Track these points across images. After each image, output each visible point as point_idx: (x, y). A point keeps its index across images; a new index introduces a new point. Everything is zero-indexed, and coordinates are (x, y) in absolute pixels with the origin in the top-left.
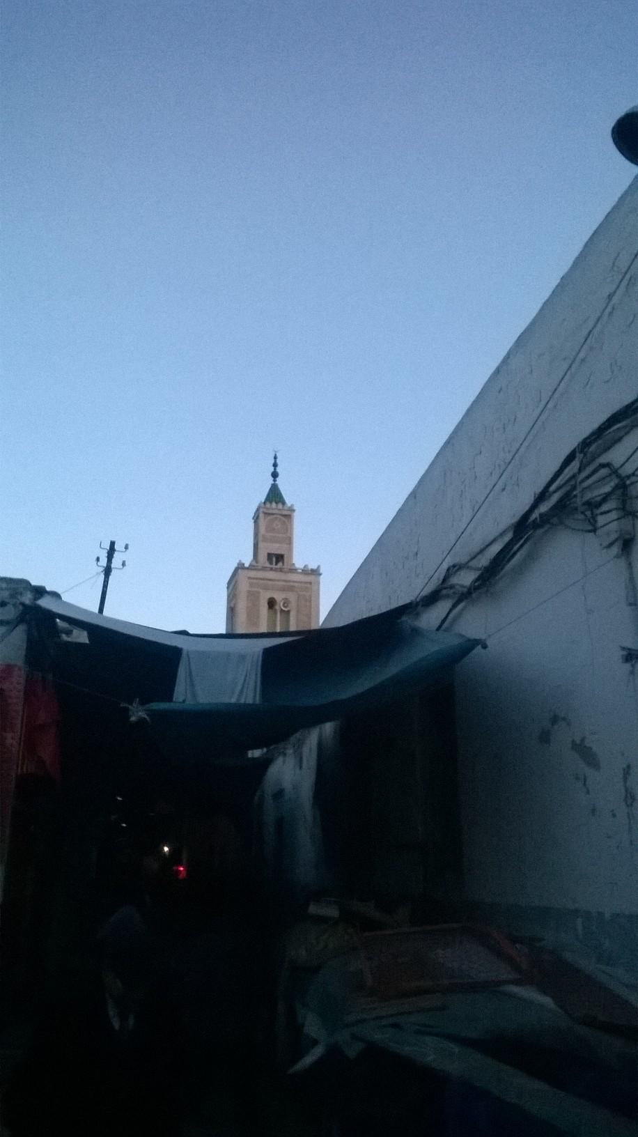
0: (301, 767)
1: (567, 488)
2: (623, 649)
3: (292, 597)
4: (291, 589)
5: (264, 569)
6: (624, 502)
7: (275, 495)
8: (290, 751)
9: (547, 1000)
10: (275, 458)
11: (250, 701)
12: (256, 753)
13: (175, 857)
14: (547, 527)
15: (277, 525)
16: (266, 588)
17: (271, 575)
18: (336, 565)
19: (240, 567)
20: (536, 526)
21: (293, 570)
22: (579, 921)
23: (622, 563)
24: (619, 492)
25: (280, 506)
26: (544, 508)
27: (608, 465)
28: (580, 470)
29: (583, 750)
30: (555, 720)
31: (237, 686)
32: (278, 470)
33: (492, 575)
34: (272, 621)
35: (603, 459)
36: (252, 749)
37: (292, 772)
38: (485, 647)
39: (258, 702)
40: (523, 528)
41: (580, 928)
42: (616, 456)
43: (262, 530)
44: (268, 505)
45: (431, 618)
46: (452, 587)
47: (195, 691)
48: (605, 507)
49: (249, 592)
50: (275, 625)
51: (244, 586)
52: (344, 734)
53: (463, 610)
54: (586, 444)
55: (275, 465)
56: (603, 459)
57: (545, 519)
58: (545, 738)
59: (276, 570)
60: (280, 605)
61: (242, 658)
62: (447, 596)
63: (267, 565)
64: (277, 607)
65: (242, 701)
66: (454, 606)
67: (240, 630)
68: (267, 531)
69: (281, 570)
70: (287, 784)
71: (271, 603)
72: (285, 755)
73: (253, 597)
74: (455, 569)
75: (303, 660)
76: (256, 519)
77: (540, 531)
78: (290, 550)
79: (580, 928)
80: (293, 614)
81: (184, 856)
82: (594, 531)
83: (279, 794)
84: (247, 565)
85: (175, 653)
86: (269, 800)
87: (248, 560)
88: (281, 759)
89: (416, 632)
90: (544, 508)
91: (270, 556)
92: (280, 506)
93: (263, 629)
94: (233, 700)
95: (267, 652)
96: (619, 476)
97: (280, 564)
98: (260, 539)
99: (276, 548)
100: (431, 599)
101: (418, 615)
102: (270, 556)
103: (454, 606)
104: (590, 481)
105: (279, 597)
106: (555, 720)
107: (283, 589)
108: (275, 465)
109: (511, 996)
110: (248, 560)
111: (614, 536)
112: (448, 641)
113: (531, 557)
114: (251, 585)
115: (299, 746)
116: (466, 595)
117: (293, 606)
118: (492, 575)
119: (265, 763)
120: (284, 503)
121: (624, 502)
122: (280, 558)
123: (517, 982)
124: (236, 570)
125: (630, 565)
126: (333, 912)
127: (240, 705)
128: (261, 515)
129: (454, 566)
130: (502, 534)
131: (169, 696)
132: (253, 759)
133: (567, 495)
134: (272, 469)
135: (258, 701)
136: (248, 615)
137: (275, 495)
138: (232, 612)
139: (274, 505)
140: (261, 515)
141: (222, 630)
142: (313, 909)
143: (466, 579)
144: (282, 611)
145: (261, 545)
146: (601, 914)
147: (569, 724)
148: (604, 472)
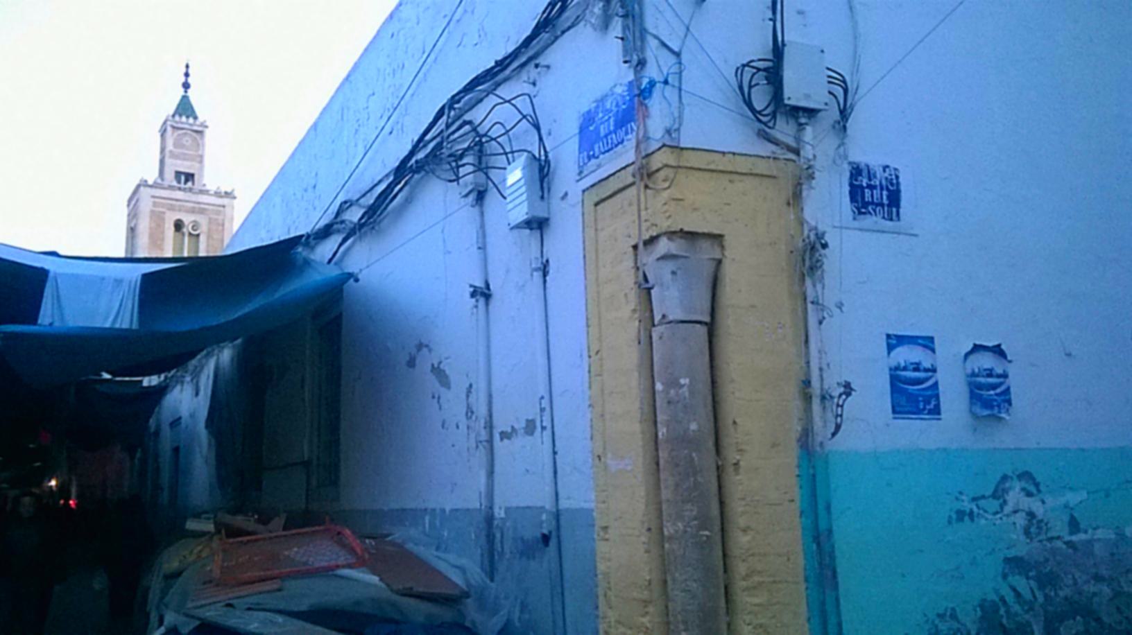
0: (197, 394)
1: (438, 139)
2: (471, 286)
3: (203, 221)
4: (202, 212)
5: (171, 188)
6: (480, 158)
7: (185, 108)
8: (188, 379)
9: (375, 579)
10: (187, 66)
11: (125, 326)
12: (150, 381)
13: (63, 490)
14: (423, 173)
15: (187, 141)
16: (172, 208)
17: (179, 195)
18: (247, 190)
19: (143, 184)
20: (420, 167)
21: (206, 192)
22: (427, 519)
23: (476, 210)
24: (477, 148)
25: (191, 120)
26: (420, 155)
27: (470, 123)
28: (448, 126)
29: (438, 371)
30: (420, 346)
31: (114, 311)
32: (190, 71)
33: (375, 213)
34: (179, 245)
35: (467, 117)
36: (150, 374)
37: (188, 400)
38: (357, 280)
39: (135, 326)
40: (402, 170)
41: (427, 521)
42: (477, 115)
43: (170, 146)
44: (177, 118)
45: (327, 248)
46: (342, 222)
47: (62, 313)
48: (465, 161)
49: (152, 212)
50: (182, 249)
51: (146, 206)
52: (244, 361)
53: (353, 243)
54: (454, 100)
55: (187, 75)
56: (467, 117)
57: (420, 167)
58: (411, 363)
59: (184, 190)
60: (187, 229)
61: (118, 282)
62: (339, 231)
63: (175, 183)
64: (185, 230)
65: (117, 326)
66: (345, 240)
67: (141, 254)
68: (175, 145)
69: (190, 190)
70: (184, 411)
71: (178, 226)
72: (182, 383)
73: (158, 218)
74: (346, 205)
75: (185, 290)
76: (163, 133)
77: (416, 176)
78: (201, 169)
79: (427, 521)
80: (202, 238)
81: (74, 490)
82: (457, 179)
83: (176, 422)
84: (150, 182)
85: (41, 275)
86: (166, 431)
87: (152, 176)
88: (178, 387)
89: (307, 263)
90: (420, 155)
91: (178, 174)
92: (191, 120)
93: (169, 255)
94: (108, 325)
95: (146, 277)
96: (478, 134)
97: (189, 184)
98: (167, 154)
99: (185, 167)
100: (325, 233)
101: (313, 248)
102: (178, 174)
103: (345, 240)
104: (456, 135)
105: (187, 219)
106: (420, 346)
107: (193, 211)
108: (187, 75)
109: (342, 577)
110: (152, 176)
111: (470, 188)
112: (333, 272)
113: (408, 201)
114: (155, 204)
115: (196, 375)
116: (356, 230)
117: (203, 229)
118: (375, 213)
119: (160, 392)
120: (196, 118)
121: (480, 158)
122: (190, 177)
123: (350, 566)
124: (138, 186)
125: (482, 214)
126: (211, 527)
127: (122, 330)
128: (169, 129)
129: (345, 202)
130: (387, 176)
131: (33, 319)
132: (149, 387)
133: (439, 146)
134: (183, 79)
135: (135, 326)
136: (152, 236)
137: (185, 108)
138: (132, 231)
139: (184, 119)
140: (169, 129)
141: (121, 254)
142: (191, 525)
143: (354, 215)
144: (190, 234)
145: (168, 161)
146: (443, 511)
147: (430, 350)
148: (467, 128)
